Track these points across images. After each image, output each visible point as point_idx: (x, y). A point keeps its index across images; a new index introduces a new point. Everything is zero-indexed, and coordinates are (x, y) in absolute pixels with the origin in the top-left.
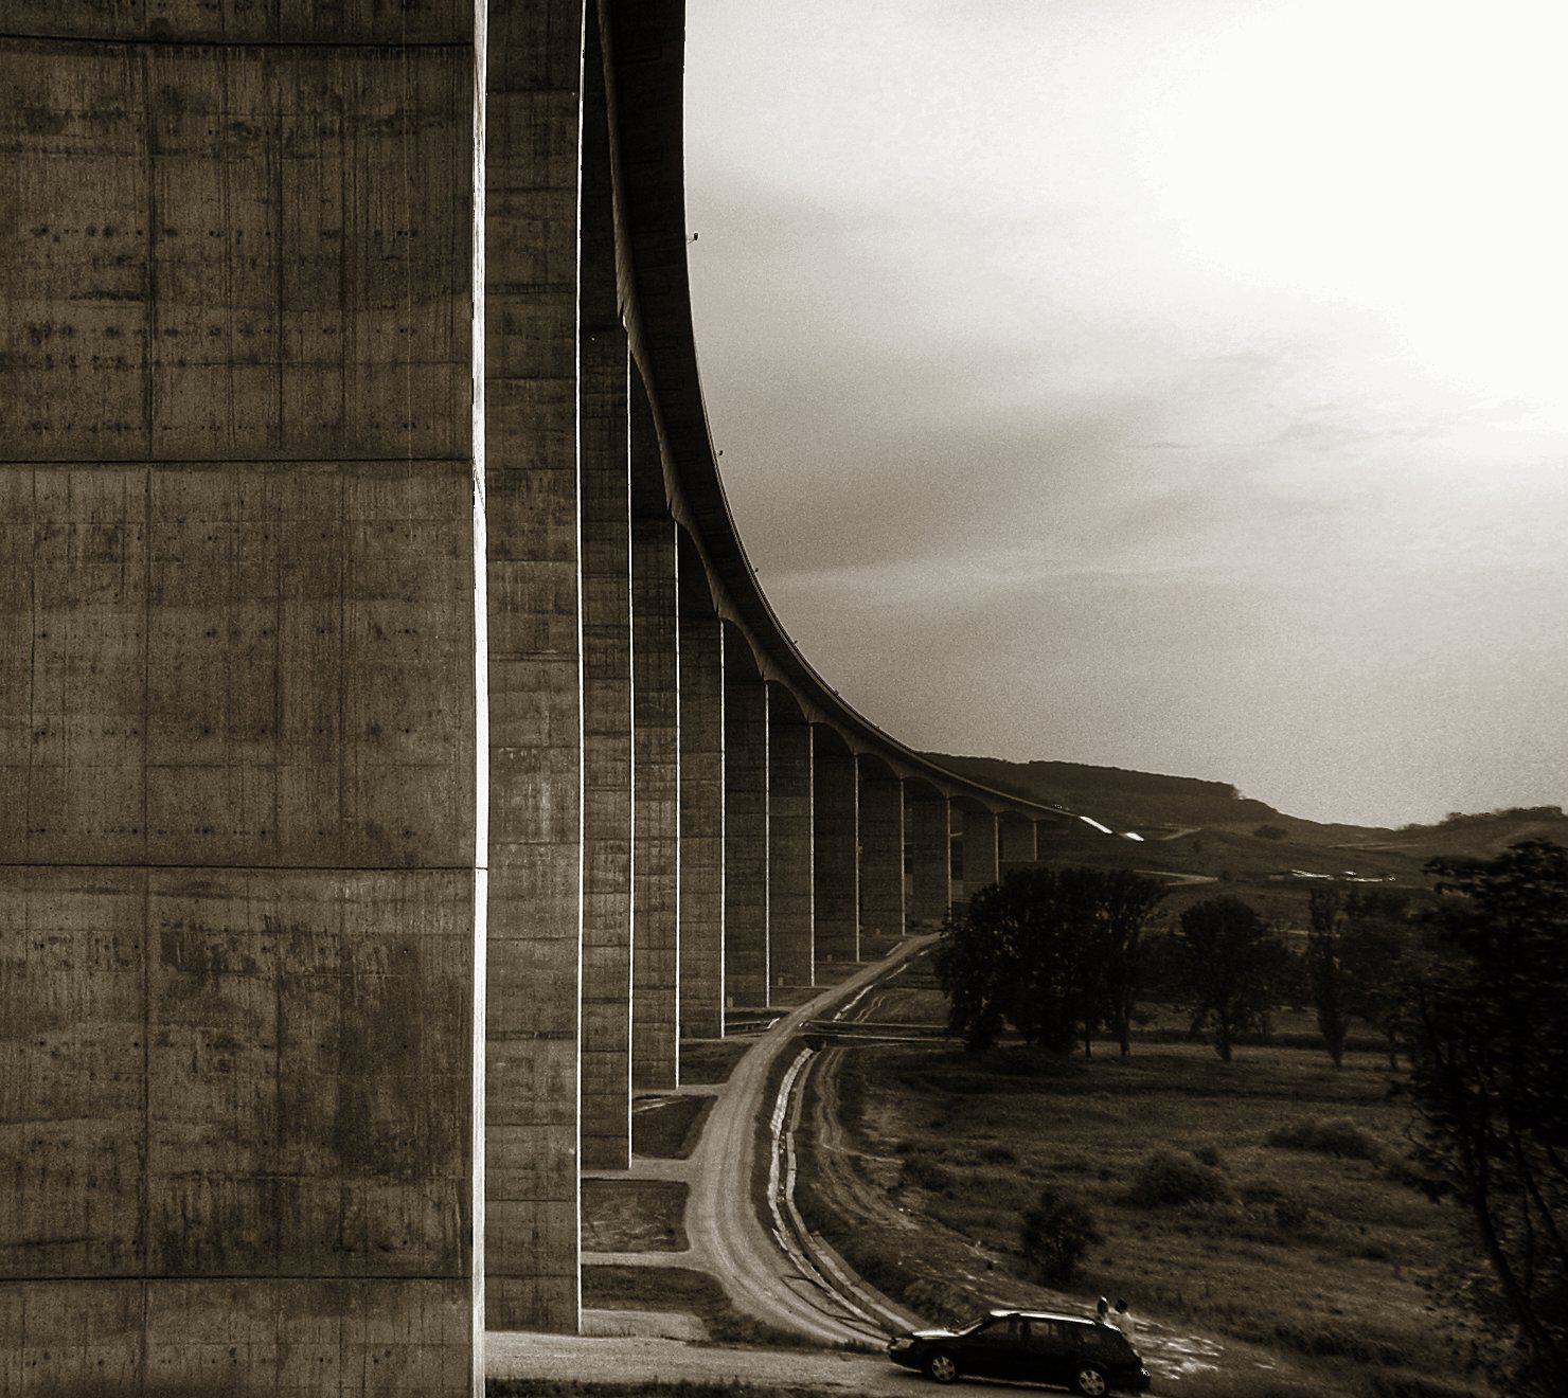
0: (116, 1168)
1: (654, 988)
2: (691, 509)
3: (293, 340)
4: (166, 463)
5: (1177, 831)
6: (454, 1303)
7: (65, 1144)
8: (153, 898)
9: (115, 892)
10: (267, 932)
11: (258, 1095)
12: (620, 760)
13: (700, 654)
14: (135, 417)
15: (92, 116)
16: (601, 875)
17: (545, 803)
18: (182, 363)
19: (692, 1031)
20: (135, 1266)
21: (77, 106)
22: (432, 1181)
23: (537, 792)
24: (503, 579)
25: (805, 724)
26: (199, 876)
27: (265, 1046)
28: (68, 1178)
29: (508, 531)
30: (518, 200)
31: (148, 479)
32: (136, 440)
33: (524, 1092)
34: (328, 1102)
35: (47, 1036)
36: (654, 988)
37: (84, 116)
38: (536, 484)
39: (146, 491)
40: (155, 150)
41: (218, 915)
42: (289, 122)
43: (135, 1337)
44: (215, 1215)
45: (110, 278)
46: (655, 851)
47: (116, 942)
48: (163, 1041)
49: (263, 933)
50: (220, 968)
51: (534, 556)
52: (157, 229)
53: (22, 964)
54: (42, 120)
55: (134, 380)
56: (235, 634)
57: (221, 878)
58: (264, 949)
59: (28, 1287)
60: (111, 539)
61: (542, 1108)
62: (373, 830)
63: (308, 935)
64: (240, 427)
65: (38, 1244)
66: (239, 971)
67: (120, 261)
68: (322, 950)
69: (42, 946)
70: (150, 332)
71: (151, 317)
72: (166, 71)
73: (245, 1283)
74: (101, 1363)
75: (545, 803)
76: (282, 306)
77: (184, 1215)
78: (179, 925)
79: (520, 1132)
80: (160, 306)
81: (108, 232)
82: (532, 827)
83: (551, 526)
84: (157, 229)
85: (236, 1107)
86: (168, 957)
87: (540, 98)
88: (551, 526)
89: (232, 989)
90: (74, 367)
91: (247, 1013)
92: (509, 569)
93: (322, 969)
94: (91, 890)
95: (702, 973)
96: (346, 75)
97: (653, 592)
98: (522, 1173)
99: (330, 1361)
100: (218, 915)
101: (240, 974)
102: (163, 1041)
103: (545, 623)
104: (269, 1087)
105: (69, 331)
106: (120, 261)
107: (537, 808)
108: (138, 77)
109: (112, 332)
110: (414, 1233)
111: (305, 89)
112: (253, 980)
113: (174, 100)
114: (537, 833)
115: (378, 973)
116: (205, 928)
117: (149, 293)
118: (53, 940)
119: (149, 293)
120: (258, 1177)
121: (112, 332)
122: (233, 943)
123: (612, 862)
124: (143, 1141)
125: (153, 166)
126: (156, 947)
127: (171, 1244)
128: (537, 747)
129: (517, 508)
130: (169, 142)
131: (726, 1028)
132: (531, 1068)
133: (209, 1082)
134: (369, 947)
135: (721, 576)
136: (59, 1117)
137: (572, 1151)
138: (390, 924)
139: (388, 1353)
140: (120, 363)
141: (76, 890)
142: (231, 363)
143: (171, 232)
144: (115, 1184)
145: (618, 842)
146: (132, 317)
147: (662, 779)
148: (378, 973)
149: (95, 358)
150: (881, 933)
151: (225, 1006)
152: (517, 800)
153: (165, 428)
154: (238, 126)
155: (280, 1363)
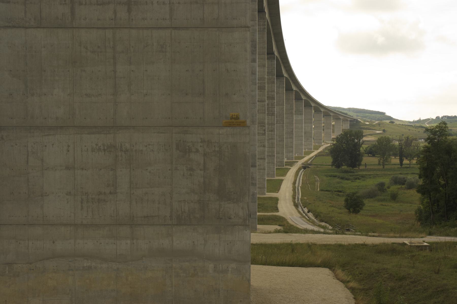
0: (165, 199)
1: (270, 156)
2: (279, 53)
4: (175, 28)
5: (376, 122)
6: (246, 231)
7: (153, 194)
10: (201, 142)
11: (199, 182)
12: (264, 107)
18: (179, 3)
19: (278, 165)
22: (241, 202)
25: (302, 99)
27: (201, 170)
31: (171, 32)
36: (270, 156)
39: (171, 35)
46: (270, 127)
49: (200, 142)
53: (142, 151)
58: (201, 146)
64: (193, 19)
65: (147, 217)
66: (194, 152)
68: (215, 146)
69: (147, 146)
73: (196, 226)
74: (163, 244)
77: (181, 211)
78: (180, 141)
85: (194, 185)
90: (152, 4)
99: (217, 244)
112: (198, 154)
115: (228, 152)
116: (186, 141)
118: (149, 145)
123: (262, 129)
131: (285, 165)
135: (285, 67)
137: (256, 192)
139: (230, 243)
141: (155, 133)
145: (263, 125)
147: (272, 111)
148: (228, 152)
149: (158, 2)
150: (318, 144)
153: (175, 19)
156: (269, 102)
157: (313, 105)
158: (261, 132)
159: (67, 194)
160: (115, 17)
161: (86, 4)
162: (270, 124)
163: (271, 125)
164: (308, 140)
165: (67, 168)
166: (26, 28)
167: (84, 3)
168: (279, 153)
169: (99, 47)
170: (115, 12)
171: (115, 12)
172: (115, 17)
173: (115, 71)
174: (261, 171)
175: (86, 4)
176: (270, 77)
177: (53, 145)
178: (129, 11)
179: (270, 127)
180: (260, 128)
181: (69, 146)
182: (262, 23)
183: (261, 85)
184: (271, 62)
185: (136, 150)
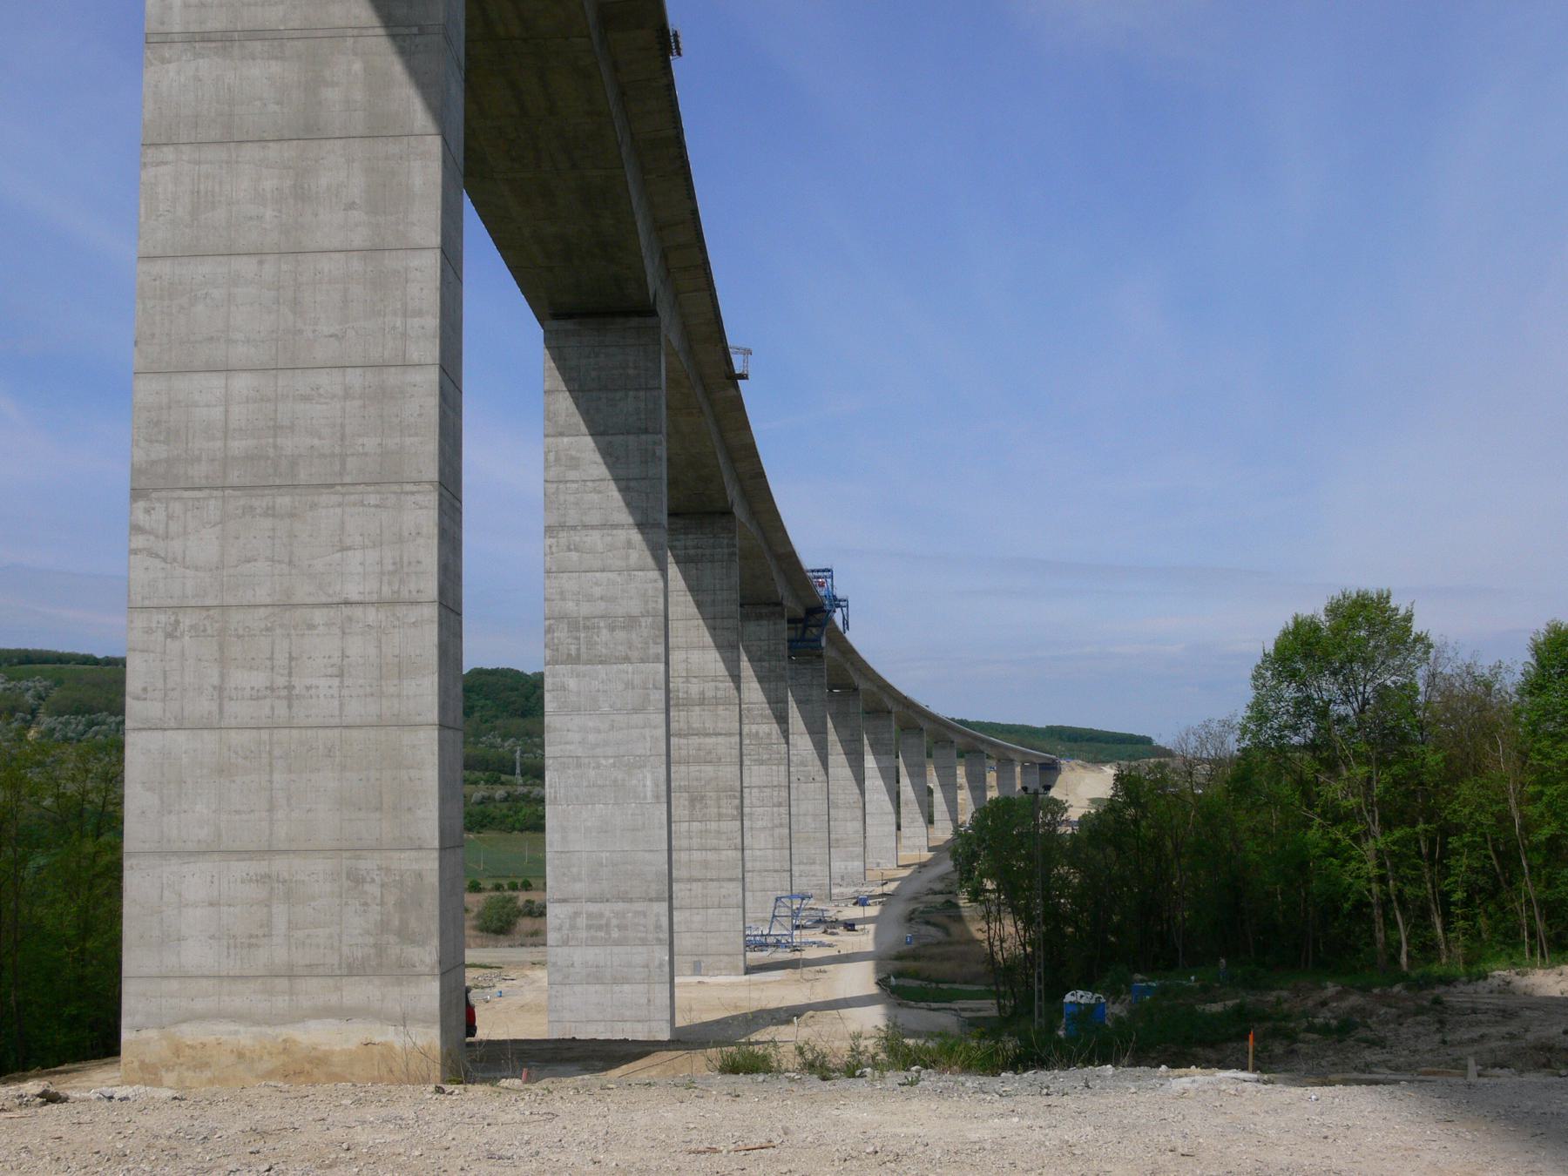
3: (384, 689)
8: (344, 860)
9: (331, 858)
13: (813, 678)
14: (337, 713)
15: (326, 625)
16: (724, 811)
17: (649, 783)
20: (338, 972)
21: (321, 623)
23: (645, 777)
24: (627, 672)
26: (358, 852)
28: (318, 946)
29: (630, 648)
30: (632, 484)
32: (336, 721)
33: (642, 928)
34: (396, 922)
35: (312, 904)
37: (323, 625)
38: (644, 624)
40: (344, 633)
41: (363, 865)
42: (383, 624)
43: (339, 993)
44: (363, 958)
45: (330, 671)
46: (775, 794)
47: (332, 874)
48: (346, 904)
50: (364, 881)
51: (643, 661)
52: (344, 656)
53: (303, 881)
54: (311, 627)
55: (336, 703)
56: (368, 780)
57: (364, 853)
59: (307, 978)
60: (330, 751)
61: (650, 936)
62: (410, 838)
63: (390, 870)
67: (332, 666)
70: (341, 687)
71: (342, 682)
72: (347, 611)
75: (649, 783)
76: (381, 678)
79: (640, 949)
80: (345, 679)
81: (329, 657)
82: (642, 795)
83: (651, 645)
84: (344, 656)
86: (348, 878)
87: (644, 437)
88: (651, 645)
89: (367, 887)
91: (372, 894)
92: (631, 668)
93: (394, 881)
94: (324, 858)
95: (818, 862)
96: (401, 611)
97: (772, 648)
98: (642, 969)
100: (363, 865)
101: (370, 883)
102: (346, 904)
103: (648, 695)
104: (379, 918)
105: (318, 687)
106: (332, 666)
107: (644, 786)
108: (339, 613)
109: (330, 687)
110: (422, 962)
111: (389, 614)
113: (350, 619)
114: (645, 798)
117: (341, 675)
119: (341, 675)
120: (375, 945)
121: (330, 687)
122: (368, 873)
124: (340, 936)
125: (343, 637)
126: (344, 876)
127: (349, 966)
128: (644, 756)
129: (634, 636)
130: (347, 631)
132: (645, 916)
133: (360, 916)
134: (408, 873)
136: (316, 928)
138: (415, 866)
140: (332, 696)
142: (366, 696)
143: (348, 657)
144: (332, 948)
146: (336, 682)
151: (366, 893)
152: (634, 782)
154: (369, 625)
155: (382, 1000)
156: (771, 729)
157: (926, 725)
158: (730, 811)
159: (210, 938)
160: (273, 714)
161: (237, 699)
162: (776, 787)
163: (777, 789)
164: (913, 822)
165: (211, 904)
166: (165, 729)
167: (235, 698)
168: (814, 863)
169: (252, 752)
170: (272, 708)
171: (272, 708)
172: (273, 714)
173: (271, 782)
174: (731, 911)
175: (237, 699)
176: (773, 663)
177: (193, 875)
178: (290, 707)
179: (775, 794)
180: (725, 801)
181: (213, 876)
182: (725, 541)
183: (727, 695)
184: (775, 624)
185: (296, 881)
